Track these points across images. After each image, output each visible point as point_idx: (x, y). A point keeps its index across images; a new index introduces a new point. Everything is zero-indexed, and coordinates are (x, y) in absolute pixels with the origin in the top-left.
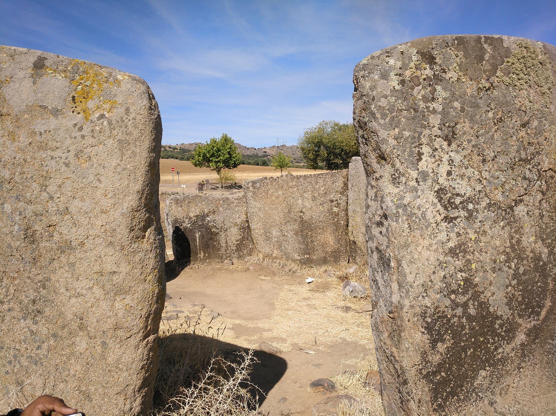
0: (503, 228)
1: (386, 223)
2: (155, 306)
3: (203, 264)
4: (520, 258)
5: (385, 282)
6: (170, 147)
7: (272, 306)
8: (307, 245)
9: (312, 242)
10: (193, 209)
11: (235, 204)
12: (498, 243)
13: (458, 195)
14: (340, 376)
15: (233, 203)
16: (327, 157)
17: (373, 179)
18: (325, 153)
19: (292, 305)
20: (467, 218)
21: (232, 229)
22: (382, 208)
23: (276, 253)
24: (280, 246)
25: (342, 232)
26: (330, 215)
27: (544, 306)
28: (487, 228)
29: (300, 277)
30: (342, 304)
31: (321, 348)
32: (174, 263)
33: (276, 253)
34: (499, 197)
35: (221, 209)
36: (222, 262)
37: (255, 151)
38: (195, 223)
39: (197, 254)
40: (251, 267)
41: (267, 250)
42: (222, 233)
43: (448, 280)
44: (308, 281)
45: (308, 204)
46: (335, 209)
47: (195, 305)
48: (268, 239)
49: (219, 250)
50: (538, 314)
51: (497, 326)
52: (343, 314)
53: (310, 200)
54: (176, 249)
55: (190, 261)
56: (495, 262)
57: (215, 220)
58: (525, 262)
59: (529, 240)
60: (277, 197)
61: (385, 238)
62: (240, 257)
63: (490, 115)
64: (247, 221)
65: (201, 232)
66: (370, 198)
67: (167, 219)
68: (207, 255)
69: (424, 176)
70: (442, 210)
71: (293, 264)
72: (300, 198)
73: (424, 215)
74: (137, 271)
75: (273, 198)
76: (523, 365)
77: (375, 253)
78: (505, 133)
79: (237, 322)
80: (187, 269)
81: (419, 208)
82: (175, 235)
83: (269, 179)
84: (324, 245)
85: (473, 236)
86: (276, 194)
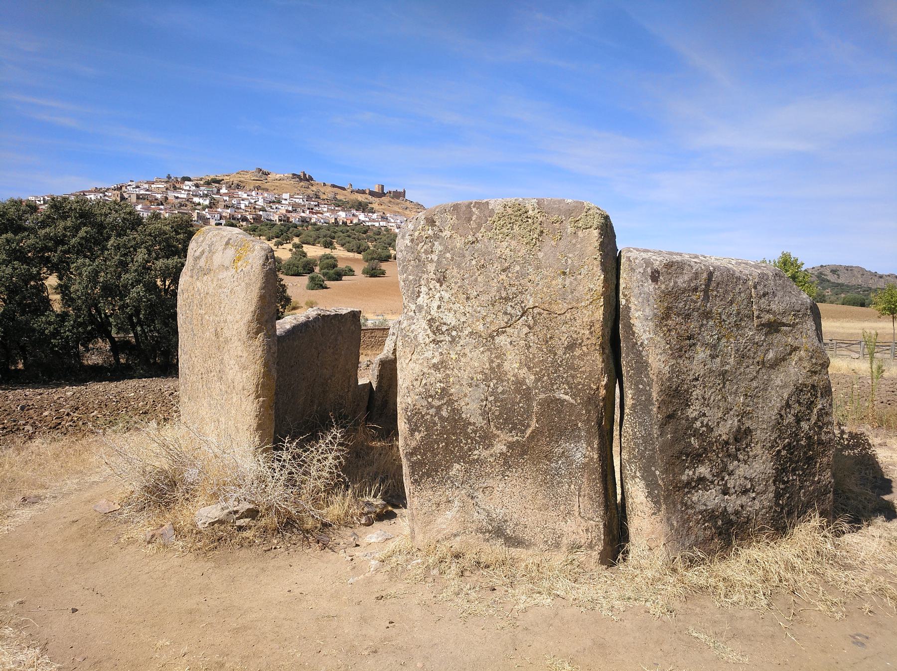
0: (483, 352)
4: (500, 380)
12: (476, 364)
13: (445, 324)
20: (450, 342)
27: (529, 426)
28: (467, 351)
34: (480, 327)
43: (429, 387)
50: (523, 432)
51: (469, 431)
56: (472, 379)
58: (505, 383)
59: (512, 365)
63: (474, 262)
69: (420, 308)
70: (431, 335)
73: (416, 337)
74: (251, 357)
76: (508, 473)
78: (487, 277)
81: (412, 332)
85: (454, 356)
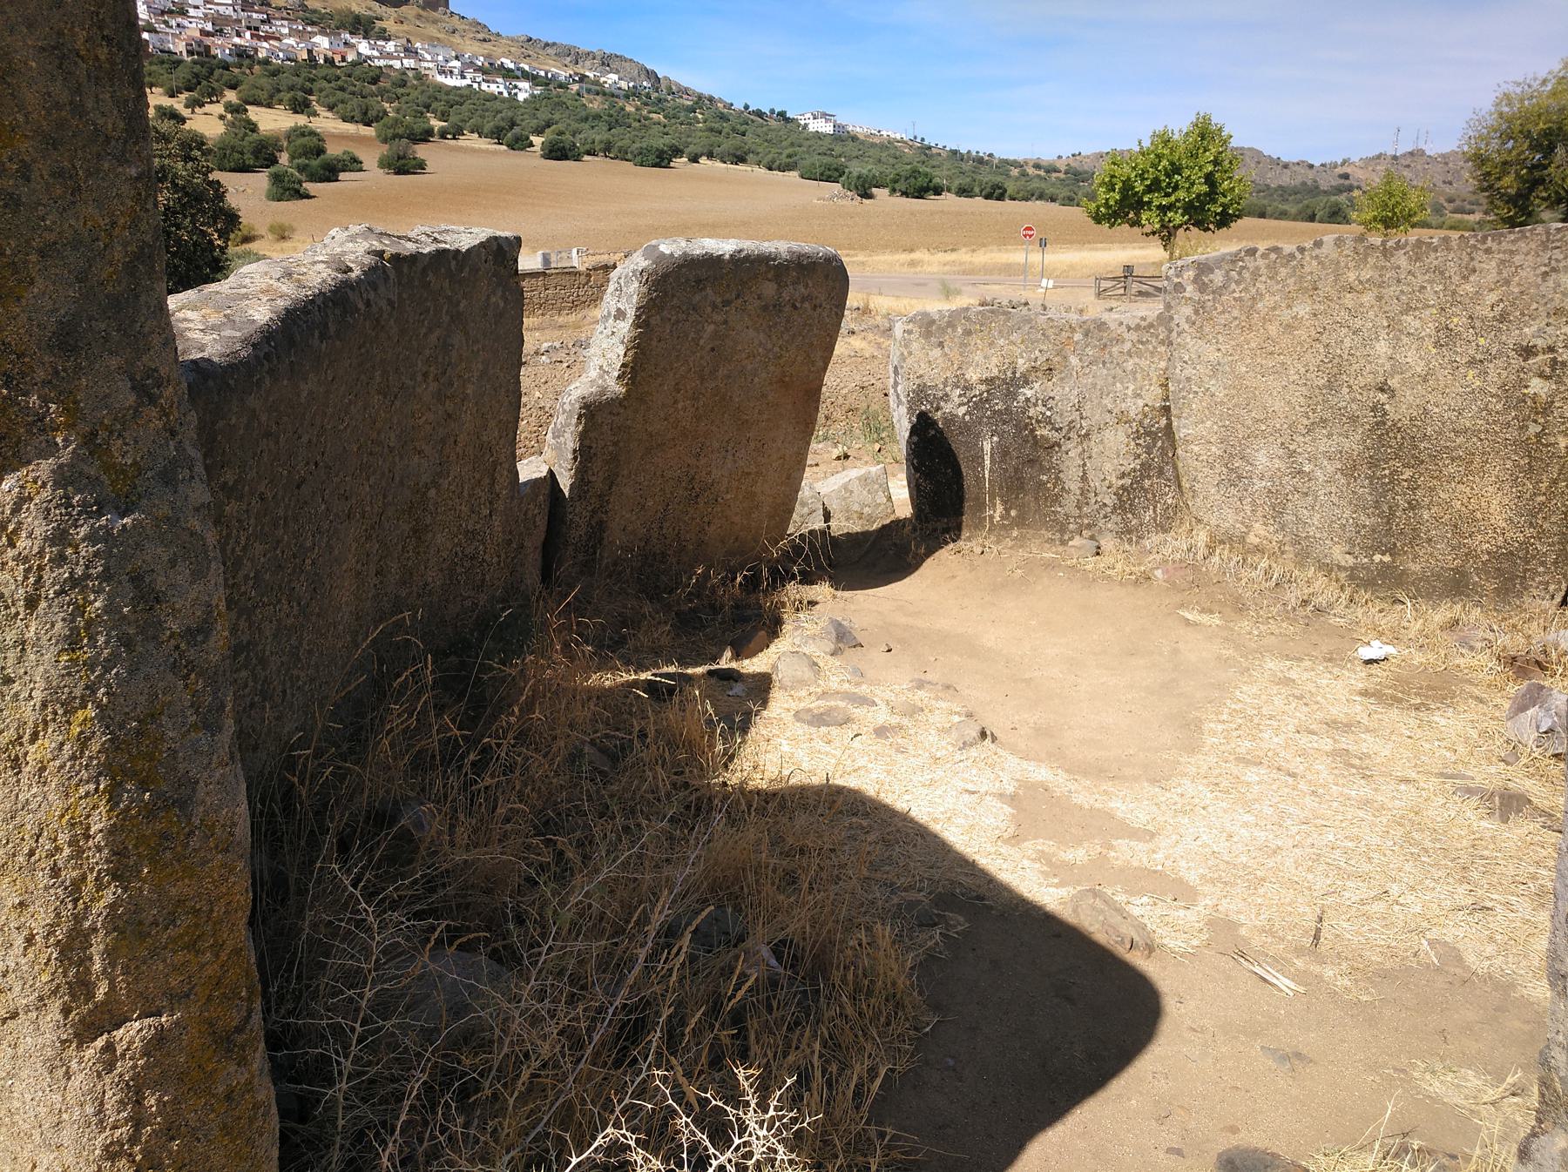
2: (109, 896)
3: (998, 542)
6: (1037, 166)
7: (1190, 731)
9: (1412, 508)
10: (978, 357)
11: (1128, 346)
15: (1119, 340)
21: (1108, 434)
23: (1259, 532)
24: (1278, 511)
25: (1555, 482)
26: (1507, 408)
30: (1489, 774)
31: (1329, 973)
32: (908, 528)
33: (1259, 532)
35: (1074, 360)
36: (1063, 543)
38: (980, 404)
39: (981, 506)
40: (1159, 573)
41: (1229, 519)
44: (1367, 653)
45: (1413, 359)
46: (1537, 386)
47: (920, 685)
48: (1235, 479)
49: (1056, 499)
52: (1484, 824)
53: (1429, 343)
54: (918, 486)
55: (959, 528)
60: (1289, 328)
62: (1126, 532)
64: (1166, 410)
65: (1001, 437)
67: (896, 384)
68: (1013, 513)
71: (1320, 582)
72: (1383, 334)
75: (1273, 329)
79: (1040, 773)
80: (945, 554)
82: (915, 439)
83: (1264, 256)
84: (1463, 525)
86: (1286, 315)
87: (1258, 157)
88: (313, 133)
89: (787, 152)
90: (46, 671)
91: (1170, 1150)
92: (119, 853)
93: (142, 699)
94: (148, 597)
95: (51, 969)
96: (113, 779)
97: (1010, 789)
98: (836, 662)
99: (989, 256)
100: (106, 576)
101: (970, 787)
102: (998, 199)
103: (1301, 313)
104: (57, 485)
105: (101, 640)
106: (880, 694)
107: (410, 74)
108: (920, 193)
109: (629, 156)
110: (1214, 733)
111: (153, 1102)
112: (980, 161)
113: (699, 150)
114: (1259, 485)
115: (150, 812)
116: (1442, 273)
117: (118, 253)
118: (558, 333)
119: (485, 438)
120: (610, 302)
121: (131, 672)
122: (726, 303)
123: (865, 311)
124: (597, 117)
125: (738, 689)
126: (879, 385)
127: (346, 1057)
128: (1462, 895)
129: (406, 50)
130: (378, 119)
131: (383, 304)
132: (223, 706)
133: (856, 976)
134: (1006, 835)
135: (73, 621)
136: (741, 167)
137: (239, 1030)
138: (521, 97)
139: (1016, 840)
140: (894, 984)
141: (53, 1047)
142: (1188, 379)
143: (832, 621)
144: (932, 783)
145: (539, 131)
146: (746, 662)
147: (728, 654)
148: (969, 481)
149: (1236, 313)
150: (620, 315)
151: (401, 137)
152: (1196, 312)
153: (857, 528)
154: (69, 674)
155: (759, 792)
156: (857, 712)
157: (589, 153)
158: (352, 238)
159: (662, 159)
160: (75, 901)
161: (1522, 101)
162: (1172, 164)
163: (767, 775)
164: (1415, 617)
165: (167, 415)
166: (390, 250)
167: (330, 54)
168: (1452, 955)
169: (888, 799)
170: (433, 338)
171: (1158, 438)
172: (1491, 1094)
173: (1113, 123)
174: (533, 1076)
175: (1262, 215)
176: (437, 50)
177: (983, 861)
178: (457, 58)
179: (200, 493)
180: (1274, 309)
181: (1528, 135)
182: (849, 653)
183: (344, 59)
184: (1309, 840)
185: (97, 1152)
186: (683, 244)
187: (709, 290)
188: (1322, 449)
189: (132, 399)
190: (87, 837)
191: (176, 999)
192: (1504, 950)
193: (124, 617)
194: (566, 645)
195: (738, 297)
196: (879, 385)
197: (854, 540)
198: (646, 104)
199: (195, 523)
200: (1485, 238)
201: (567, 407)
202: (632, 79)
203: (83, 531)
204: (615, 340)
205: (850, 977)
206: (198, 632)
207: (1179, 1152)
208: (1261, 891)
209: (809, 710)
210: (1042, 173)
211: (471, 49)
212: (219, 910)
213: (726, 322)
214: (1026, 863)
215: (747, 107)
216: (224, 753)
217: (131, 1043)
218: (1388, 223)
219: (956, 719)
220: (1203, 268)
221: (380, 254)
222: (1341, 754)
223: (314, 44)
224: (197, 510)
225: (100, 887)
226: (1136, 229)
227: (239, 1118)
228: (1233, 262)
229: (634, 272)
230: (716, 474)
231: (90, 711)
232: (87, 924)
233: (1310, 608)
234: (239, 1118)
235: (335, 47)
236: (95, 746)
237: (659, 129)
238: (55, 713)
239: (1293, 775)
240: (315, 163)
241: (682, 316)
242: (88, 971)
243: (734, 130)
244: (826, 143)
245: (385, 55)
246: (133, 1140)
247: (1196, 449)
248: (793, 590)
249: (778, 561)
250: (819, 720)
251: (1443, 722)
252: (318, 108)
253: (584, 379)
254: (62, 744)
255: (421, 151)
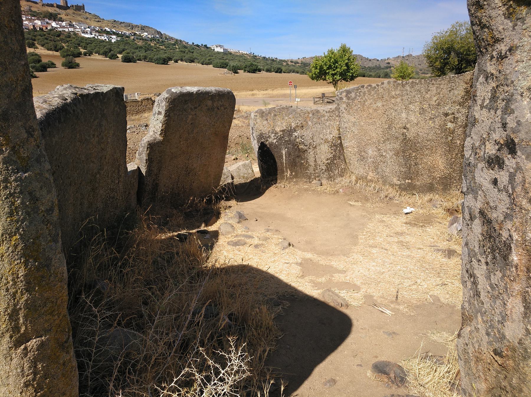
1: (510, 162)
2: (25, 297)
3: (289, 183)
5: (491, 286)
6: (292, 62)
7: (354, 239)
8: (410, 169)
9: (416, 165)
10: (279, 123)
11: (326, 118)
14: (417, 360)
15: (324, 116)
16: (458, 64)
17: (492, 57)
18: (456, 60)
19: (379, 240)
21: (322, 146)
22: (504, 126)
23: (371, 175)
24: (376, 168)
25: (457, 154)
29: (397, 205)
30: (444, 245)
31: (401, 307)
32: (260, 181)
33: (371, 175)
35: (310, 123)
36: (310, 182)
37: (378, 63)
38: (281, 138)
39: (283, 172)
40: (341, 190)
41: (361, 172)
42: (310, 150)
45: (413, 118)
46: (450, 125)
47: (268, 231)
48: (362, 159)
49: (307, 168)
55: (276, 180)
57: (304, 135)
60: (375, 110)
61: (504, 196)
62: (330, 178)
64: (340, 138)
66: (479, 102)
67: (253, 133)
68: (293, 174)
71: (391, 190)
72: (404, 111)
75: (371, 111)
77: (477, 222)
79: (309, 255)
80: (272, 188)
83: (367, 88)
84: (431, 169)
86: (375, 106)
87: (362, 58)
88: (36, 55)
89: (208, 59)
90: (3, 224)
91: (358, 365)
92: (28, 283)
93: (34, 232)
94: (34, 199)
95: (6, 323)
96: (26, 258)
97: (300, 261)
98: (240, 225)
99: (278, 91)
100: (21, 192)
101: (287, 261)
102: (280, 73)
103: (379, 105)
104: (4, 163)
105: (20, 213)
106: (255, 234)
107: (72, 33)
108: (254, 71)
109: (153, 61)
110: (362, 239)
111: (40, 366)
112: (273, 60)
113: (178, 58)
114: (370, 160)
115: (38, 269)
116: (420, 91)
117: (19, 89)
118: (132, 122)
119: (115, 157)
120: (156, 109)
121: (30, 223)
122: (196, 108)
123: (239, 111)
124: (141, 47)
125: (208, 236)
126: (245, 135)
127: (90, 361)
128: (439, 281)
129: (70, 25)
130: (60, 49)
131: (79, 111)
132: (58, 235)
133: (256, 322)
134: (299, 276)
135: (11, 207)
136: (193, 64)
137: (66, 342)
138: (113, 41)
139: (303, 277)
140: (268, 324)
141: (6, 350)
142: (346, 128)
143: (237, 212)
144: (274, 261)
145: (120, 53)
146: (210, 227)
147: (203, 225)
148: (279, 164)
149: (359, 106)
150: (160, 113)
151: (70, 55)
152: (347, 106)
153: (243, 181)
154: (10, 225)
155: (218, 269)
156: (248, 240)
157: (139, 60)
158: (65, 89)
159: (165, 62)
160: (14, 299)
161: (440, 38)
162: (335, 60)
163: (221, 263)
164: (418, 199)
165: (36, 141)
166: (79, 93)
167: (41, 27)
168: (437, 299)
169: (260, 267)
170: (96, 123)
171: (338, 147)
172: (451, 338)
173: (315, 47)
174: (156, 359)
175: (364, 76)
176: (81, 25)
177: (294, 284)
178: (89, 28)
179: (48, 166)
180: (371, 104)
181: (443, 49)
182: (244, 222)
183: (47, 28)
184: (393, 269)
185: (22, 385)
186: (180, 89)
187: (189, 104)
188: (388, 148)
189: (26, 135)
190: (18, 278)
191: (47, 331)
192: (451, 296)
193: (27, 206)
194: (148, 225)
195: (199, 106)
196: (245, 135)
197: (242, 185)
198: (158, 43)
199: (47, 175)
200: (432, 80)
201: (143, 145)
202: (153, 34)
203: (13, 178)
204: (158, 121)
205: (254, 323)
206: (50, 210)
207: (361, 365)
208: (379, 285)
209: (232, 241)
210: (293, 64)
211: (93, 24)
212: (59, 302)
213: (195, 114)
214: (307, 284)
215: (193, 43)
216: (59, 249)
217: (33, 346)
218: (403, 77)
219: (280, 240)
220: (348, 92)
221: (76, 94)
222: (401, 243)
223: (35, 23)
224: (47, 171)
225: (22, 294)
226: (325, 81)
227: (67, 371)
228: (357, 90)
229: (163, 98)
230: (195, 165)
231: (18, 236)
232: (18, 307)
233: (388, 198)
234: (67, 371)
235: (43, 24)
236: (19, 248)
237: (163, 52)
238: (6, 237)
239: (387, 250)
240: (38, 65)
241: (181, 113)
242: (18, 323)
243: (189, 51)
244: (221, 55)
245: (62, 27)
246: (34, 380)
247: (350, 150)
248: (223, 203)
249: (217, 194)
250: (236, 244)
251: (430, 230)
252: (38, 46)
253: (148, 135)
254: (9, 248)
255: (77, 60)
